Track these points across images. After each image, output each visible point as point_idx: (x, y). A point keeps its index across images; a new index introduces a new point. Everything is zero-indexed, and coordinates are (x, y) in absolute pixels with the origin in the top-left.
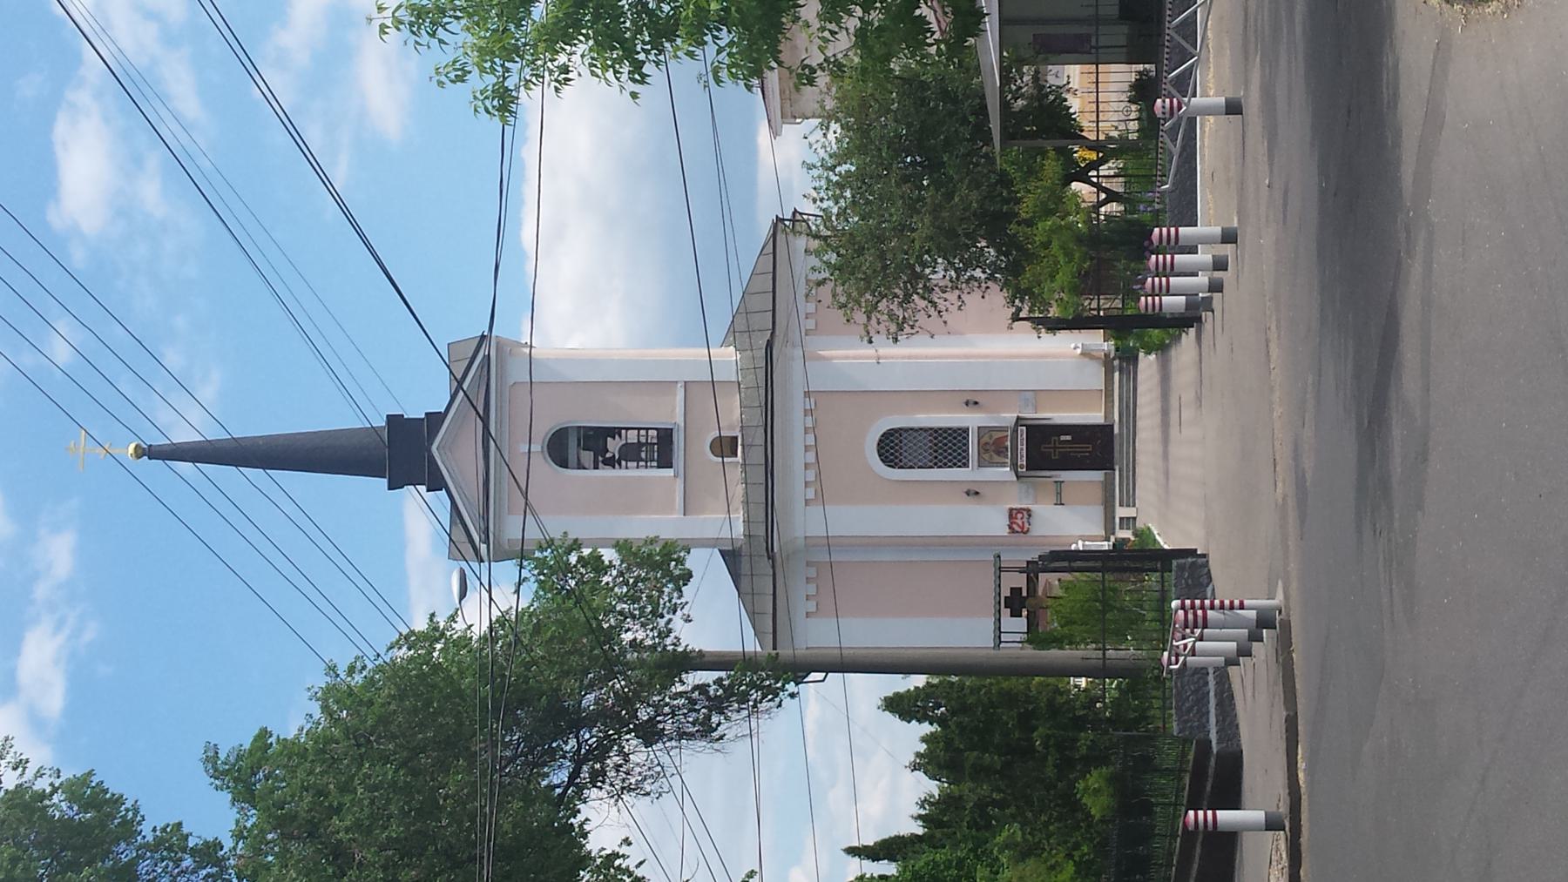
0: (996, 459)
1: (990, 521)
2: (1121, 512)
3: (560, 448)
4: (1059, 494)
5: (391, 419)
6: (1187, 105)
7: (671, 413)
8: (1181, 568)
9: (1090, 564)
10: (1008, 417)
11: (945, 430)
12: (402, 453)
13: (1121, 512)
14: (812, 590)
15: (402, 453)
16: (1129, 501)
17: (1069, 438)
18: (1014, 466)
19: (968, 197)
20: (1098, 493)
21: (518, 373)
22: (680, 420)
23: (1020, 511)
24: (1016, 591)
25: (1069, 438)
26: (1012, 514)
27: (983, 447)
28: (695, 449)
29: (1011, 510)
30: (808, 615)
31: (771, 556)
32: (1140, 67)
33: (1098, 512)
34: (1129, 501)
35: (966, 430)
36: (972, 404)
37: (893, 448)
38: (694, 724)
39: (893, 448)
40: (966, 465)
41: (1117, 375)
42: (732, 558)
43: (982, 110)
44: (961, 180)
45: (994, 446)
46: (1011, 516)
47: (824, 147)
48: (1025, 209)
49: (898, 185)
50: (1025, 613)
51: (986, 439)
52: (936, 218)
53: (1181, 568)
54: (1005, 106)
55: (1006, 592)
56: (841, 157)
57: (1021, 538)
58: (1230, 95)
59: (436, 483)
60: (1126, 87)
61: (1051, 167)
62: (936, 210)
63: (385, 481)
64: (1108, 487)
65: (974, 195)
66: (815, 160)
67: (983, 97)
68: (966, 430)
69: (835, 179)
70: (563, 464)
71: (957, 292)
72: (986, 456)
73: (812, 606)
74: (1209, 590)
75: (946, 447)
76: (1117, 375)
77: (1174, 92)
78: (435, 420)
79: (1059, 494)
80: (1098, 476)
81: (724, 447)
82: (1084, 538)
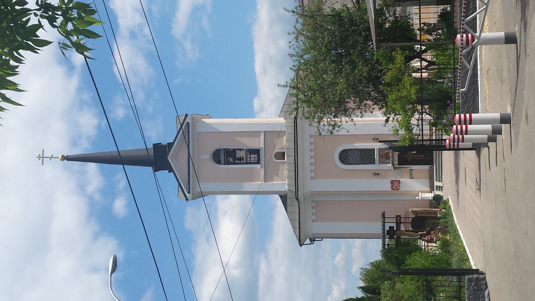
0: (386, 161)
1: (384, 185)
2: (436, 184)
4: (411, 174)
6: (479, 38)
7: (259, 143)
8: (470, 280)
11: (365, 150)
13: (436, 184)
14: (314, 211)
17: (415, 152)
18: (393, 164)
19: (363, 69)
20: (427, 174)
22: (262, 145)
23: (395, 181)
24: (391, 228)
25: (415, 152)
26: (392, 182)
27: (381, 156)
29: (392, 181)
30: (313, 221)
31: (297, 199)
32: (442, 7)
33: (427, 181)
35: (374, 150)
37: (346, 157)
39: (346, 157)
40: (374, 163)
42: (284, 198)
43: (368, 29)
44: (359, 62)
46: (392, 183)
47: (297, 47)
48: (387, 78)
49: (330, 64)
50: (395, 237)
51: (382, 153)
52: (347, 80)
53: (470, 280)
54: (379, 26)
55: (387, 228)
56: (306, 51)
57: (395, 192)
58: (511, 31)
59: (171, 170)
60: (436, 16)
61: (399, 58)
62: (348, 75)
63: (167, 171)
64: (431, 171)
65: (365, 69)
66: (293, 52)
67: (369, 23)
68: (374, 150)
69: (302, 61)
70: (219, 163)
71: (360, 111)
72: (382, 160)
73: (314, 218)
74: (486, 292)
75: (366, 156)
77: (468, 29)
78: (170, 145)
79: (411, 174)
80: (427, 167)
81: (281, 156)
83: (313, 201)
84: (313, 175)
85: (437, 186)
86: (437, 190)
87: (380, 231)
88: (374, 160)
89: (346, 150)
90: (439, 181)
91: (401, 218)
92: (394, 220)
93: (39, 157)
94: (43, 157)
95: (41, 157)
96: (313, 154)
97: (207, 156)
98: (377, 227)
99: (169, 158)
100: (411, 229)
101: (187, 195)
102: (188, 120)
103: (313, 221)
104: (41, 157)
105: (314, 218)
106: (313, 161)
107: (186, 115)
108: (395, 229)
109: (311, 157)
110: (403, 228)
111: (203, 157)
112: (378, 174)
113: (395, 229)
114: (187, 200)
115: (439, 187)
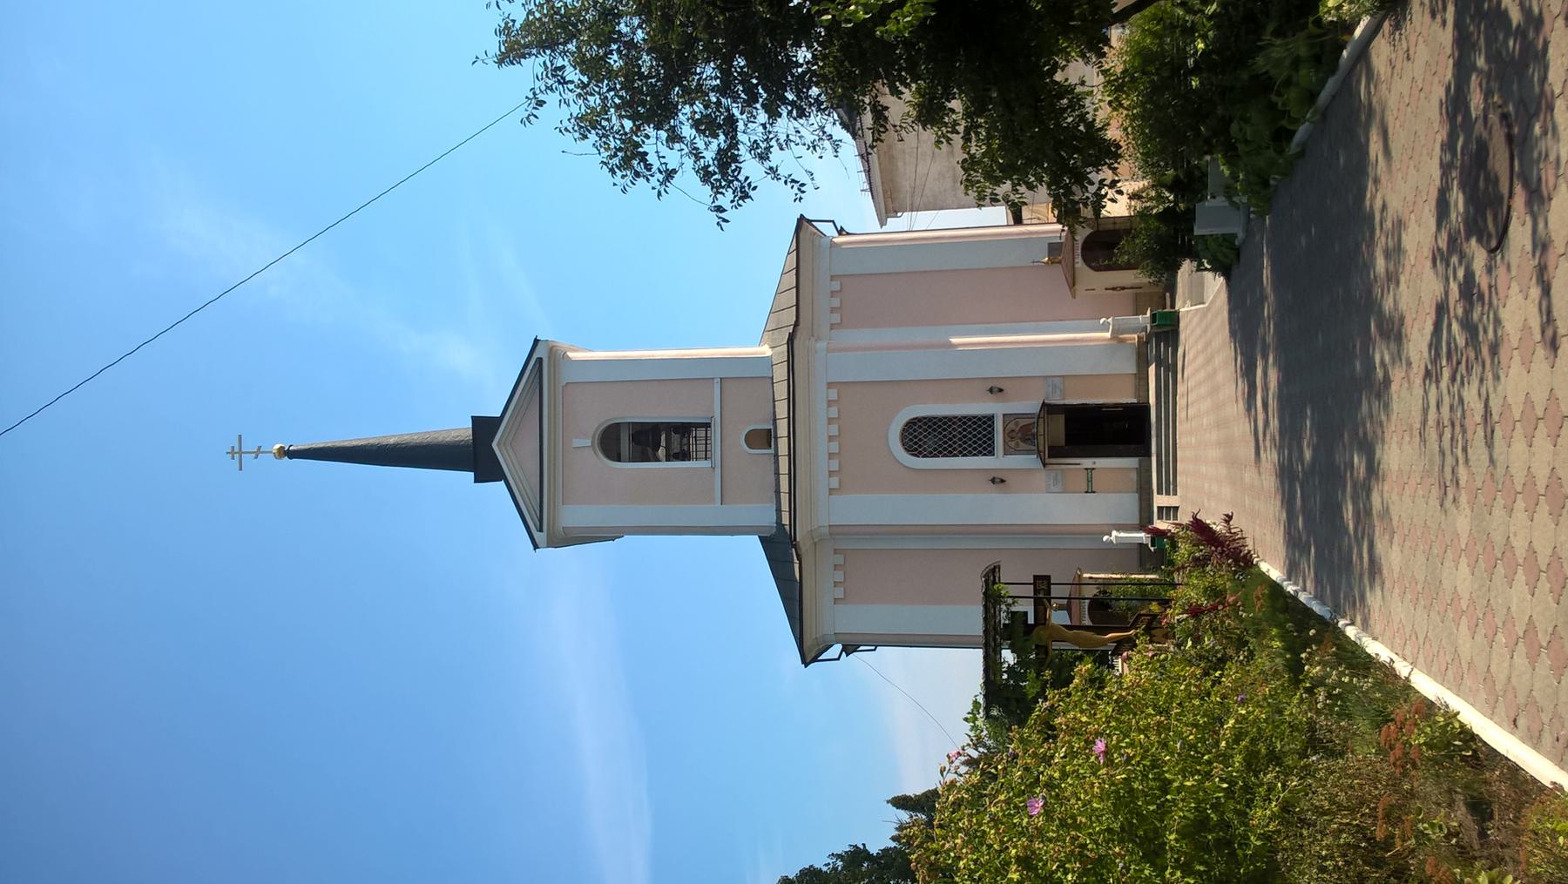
0: (1023, 446)
2: (1160, 500)
3: (612, 442)
4: (1090, 481)
5: (476, 421)
9: (785, 506)
10: (1031, 406)
11: (970, 418)
12: (476, 453)
13: (1160, 500)
14: (839, 576)
15: (476, 453)
16: (1169, 487)
21: (567, 376)
27: (1009, 435)
28: (729, 440)
30: (836, 601)
34: (1169, 487)
36: (996, 391)
38: (1111, 693)
40: (991, 453)
41: (1152, 369)
45: (1023, 434)
51: (1012, 426)
63: (472, 474)
72: (1012, 444)
73: (839, 593)
75: (966, 436)
76: (1152, 369)
79: (1090, 481)
80: (1131, 463)
82: (1120, 528)
83: (836, 551)
84: (835, 482)
85: (1160, 509)
86: (1160, 518)
87: (978, 628)
88: (992, 445)
89: (919, 420)
90: (1168, 493)
91: (1049, 584)
92: (1030, 591)
93: (232, 453)
94: (241, 452)
95: (237, 453)
96: (834, 430)
97: (585, 440)
98: (972, 619)
99: (494, 445)
100: (1087, 622)
101: (536, 534)
102: (541, 352)
103: (836, 601)
104: (237, 453)
105: (839, 593)
106: (834, 447)
107: (536, 341)
108: (1031, 620)
109: (831, 438)
110: (1058, 618)
111: (577, 443)
112: (1003, 481)
113: (1031, 620)
114: (536, 547)
115: (1168, 508)
